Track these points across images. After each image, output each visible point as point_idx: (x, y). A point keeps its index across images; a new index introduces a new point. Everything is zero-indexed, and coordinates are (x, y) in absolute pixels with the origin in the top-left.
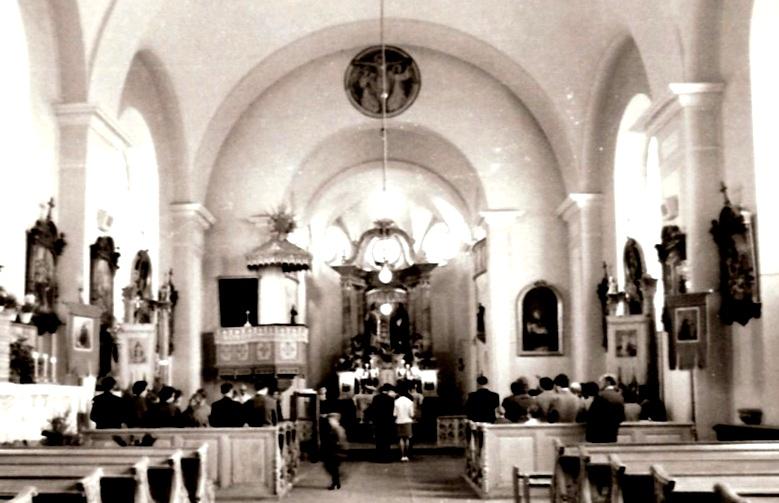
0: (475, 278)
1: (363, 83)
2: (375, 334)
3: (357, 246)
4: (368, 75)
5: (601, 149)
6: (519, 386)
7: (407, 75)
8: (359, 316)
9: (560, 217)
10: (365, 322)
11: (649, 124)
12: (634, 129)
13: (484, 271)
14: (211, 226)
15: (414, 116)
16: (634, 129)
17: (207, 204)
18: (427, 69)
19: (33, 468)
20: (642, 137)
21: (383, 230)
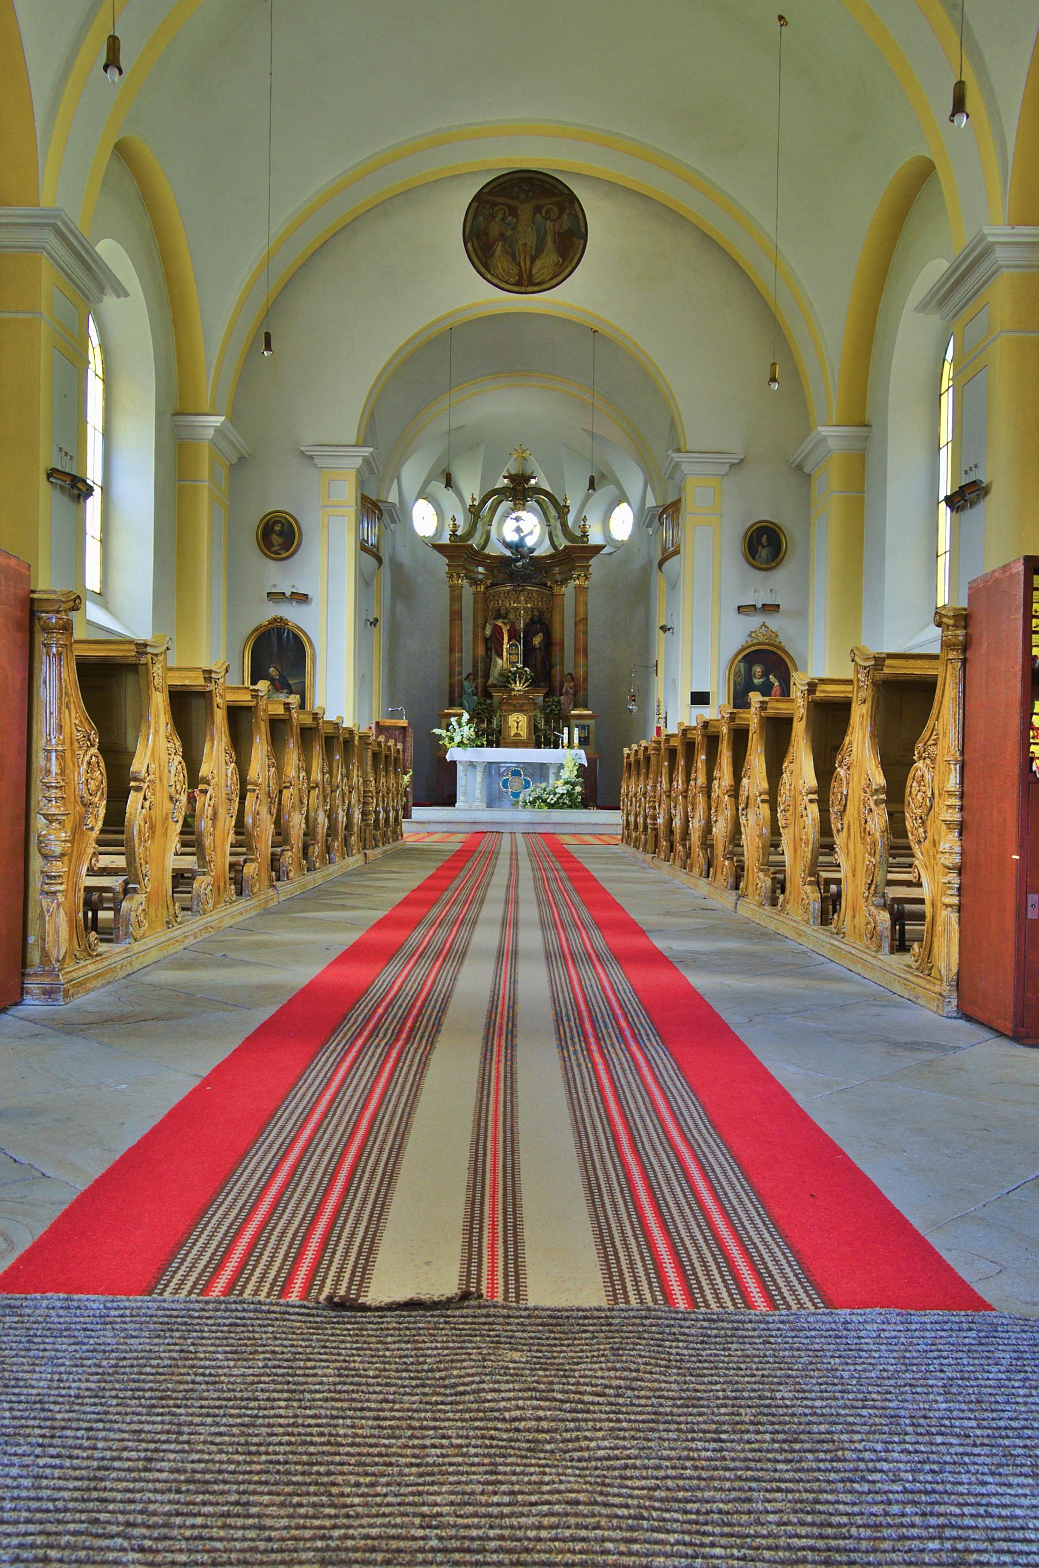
0: (661, 564)
1: (494, 229)
2: (501, 657)
3: (475, 512)
4: (503, 220)
5: (518, 687)
6: (439, 786)
7: (566, 222)
8: (475, 626)
9: (799, 468)
10: (486, 640)
11: (941, 304)
12: (923, 307)
13: (676, 552)
14: (242, 459)
15: (573, 296)
16: (923, 307)
17: (234, 417)
18: (600, 217)
19: (911, 663)
20: (933, 321)
21: (520, 490)
